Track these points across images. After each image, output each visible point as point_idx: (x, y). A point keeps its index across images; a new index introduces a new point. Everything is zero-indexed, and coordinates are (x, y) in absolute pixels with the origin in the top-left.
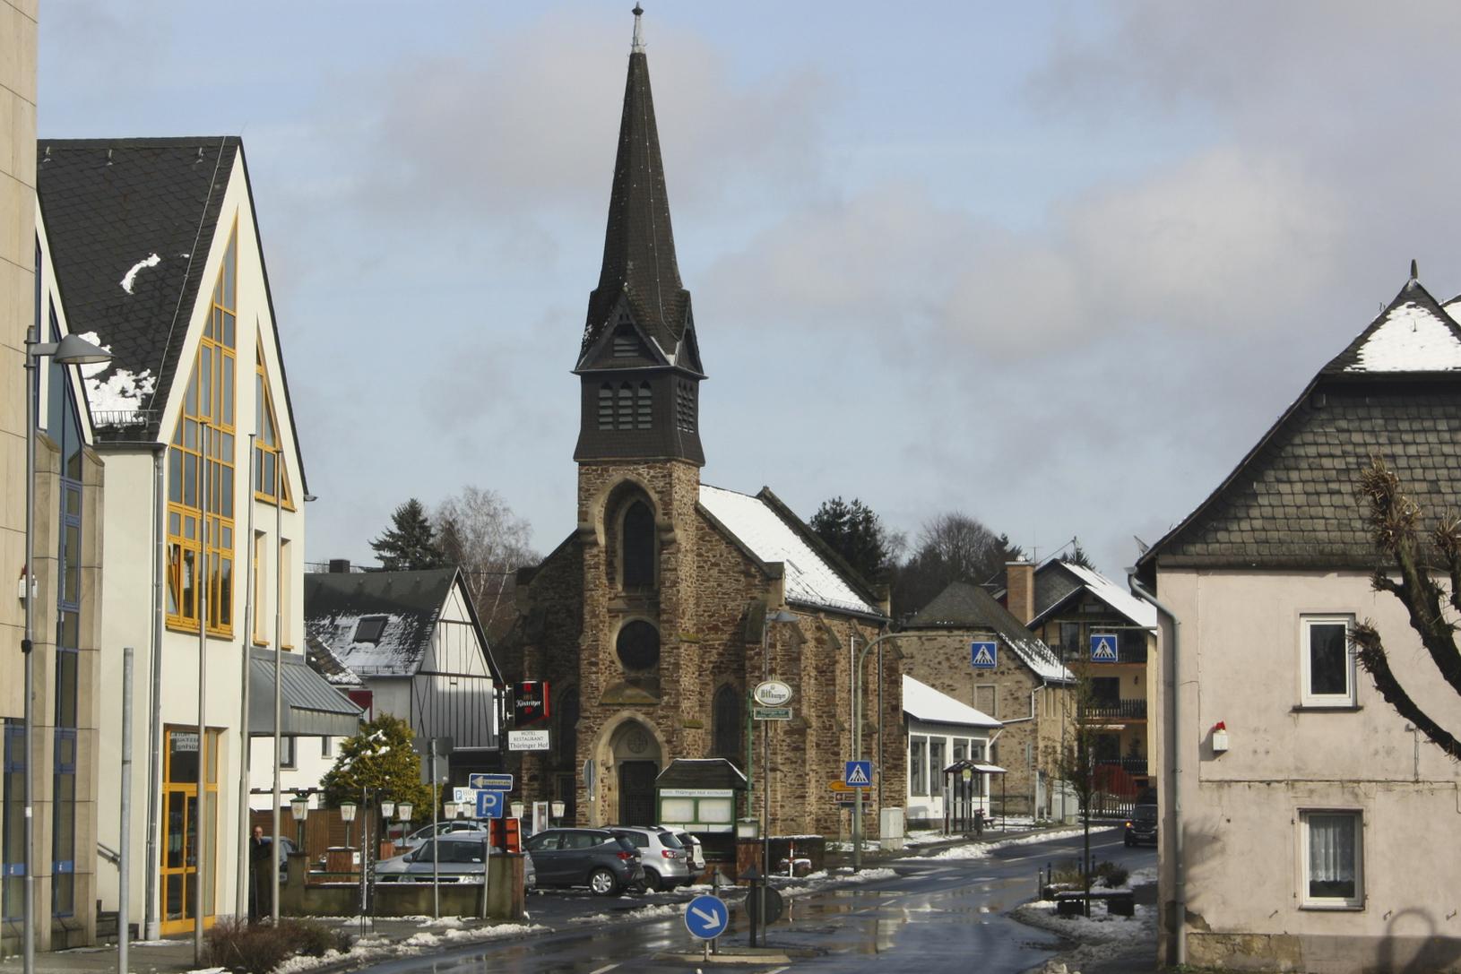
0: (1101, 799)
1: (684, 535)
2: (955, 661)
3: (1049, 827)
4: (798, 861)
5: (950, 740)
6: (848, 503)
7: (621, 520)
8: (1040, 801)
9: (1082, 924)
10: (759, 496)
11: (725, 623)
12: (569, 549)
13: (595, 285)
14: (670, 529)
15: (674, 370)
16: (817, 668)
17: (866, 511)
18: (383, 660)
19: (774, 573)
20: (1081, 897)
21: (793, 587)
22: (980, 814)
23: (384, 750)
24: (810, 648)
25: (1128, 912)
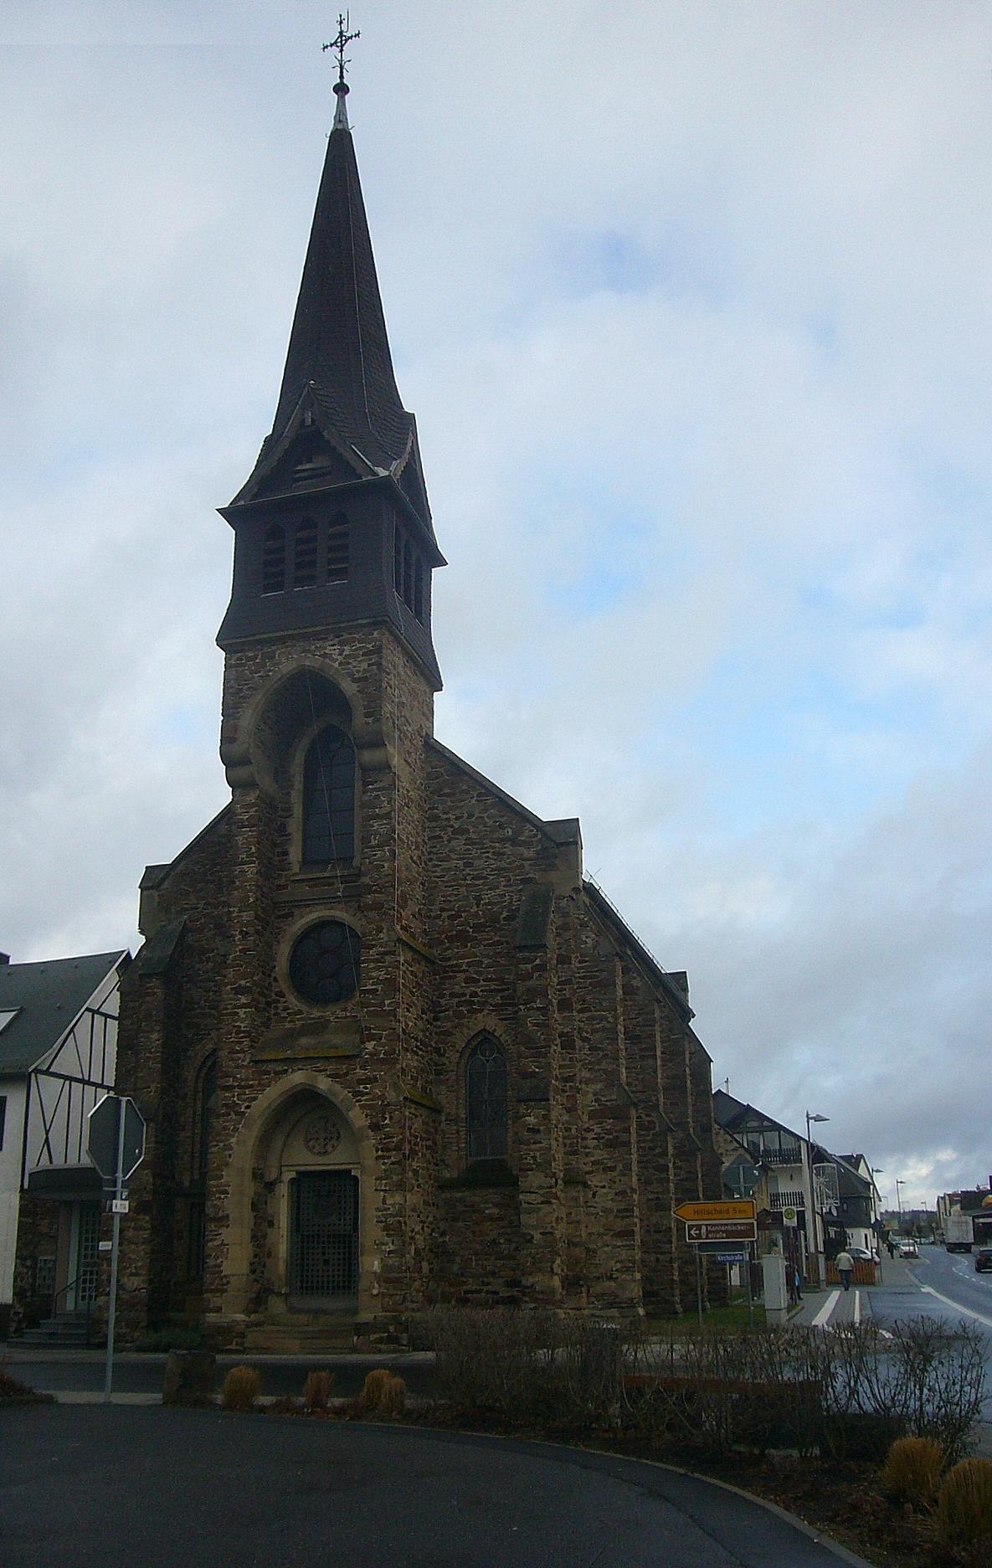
7: (299, 759)
11: (478, 928)
14: (379, 743)
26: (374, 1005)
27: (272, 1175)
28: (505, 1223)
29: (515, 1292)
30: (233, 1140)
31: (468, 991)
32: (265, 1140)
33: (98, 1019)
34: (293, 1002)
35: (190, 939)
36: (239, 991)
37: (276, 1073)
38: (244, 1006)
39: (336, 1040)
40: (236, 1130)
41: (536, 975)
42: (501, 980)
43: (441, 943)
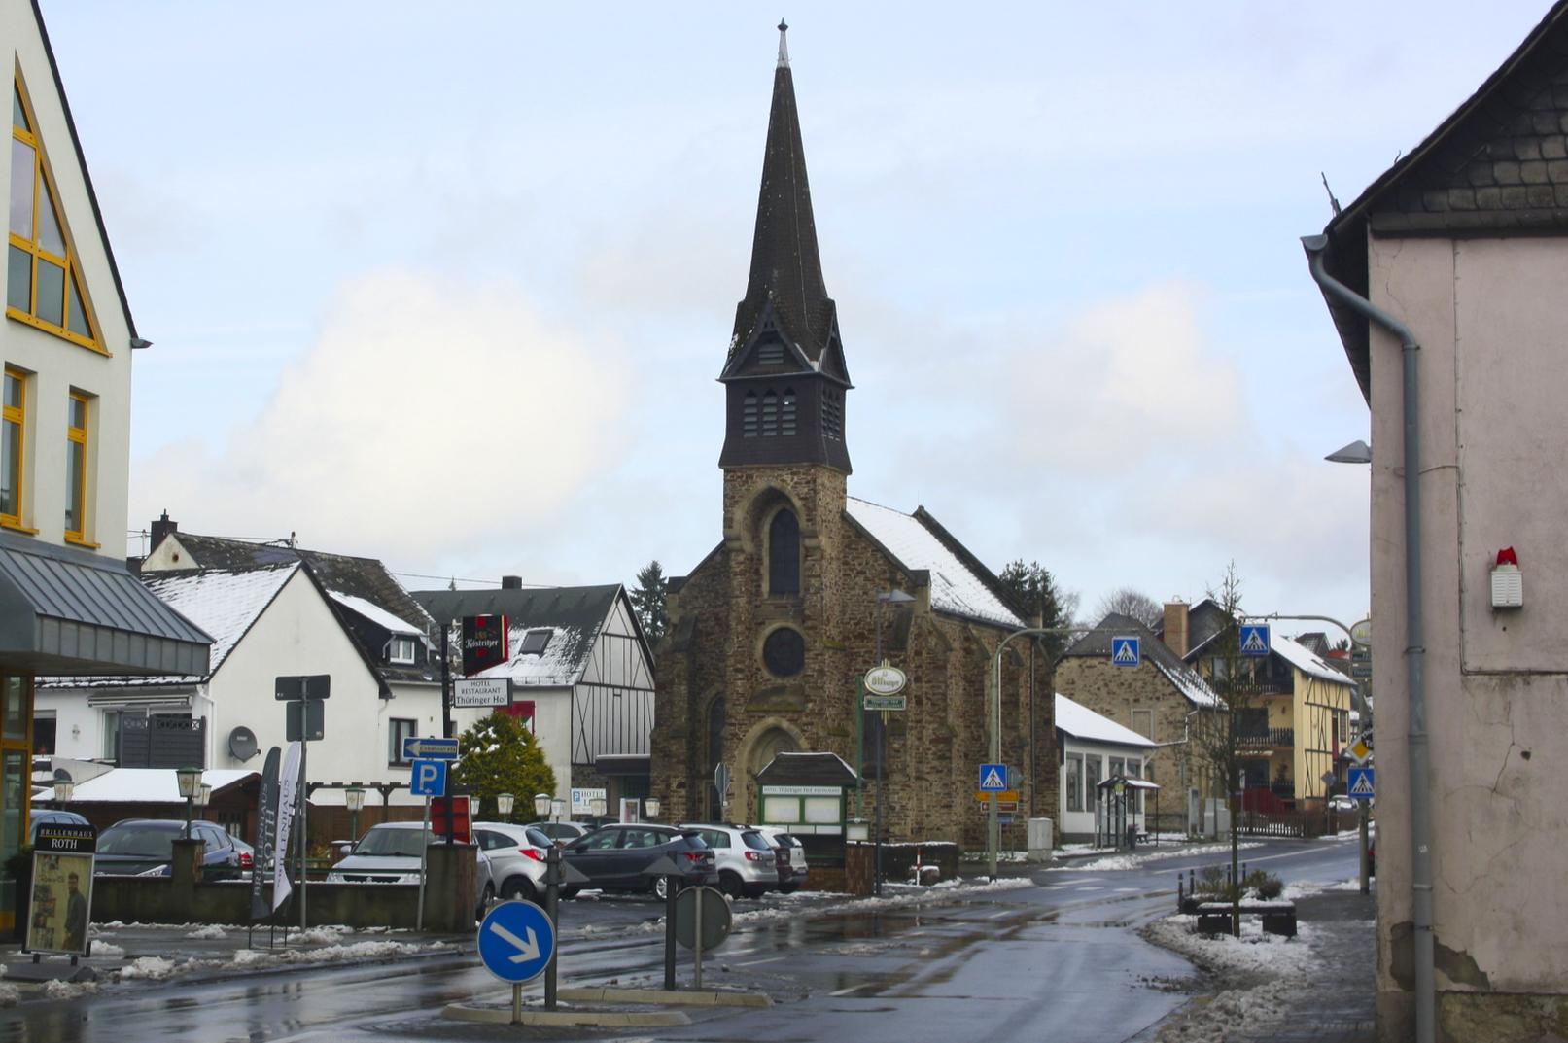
0: (1251, 817)
1: (827, 543)
2: (1113, 687)
3: (1201, 842)
4: (925, 868)
5: (1106, 758)
6: (1028, 566)
7: (766, 528)
8: (1193, 818)
9: (1227, 949)
10: (915, 516)
12: (718, 558)
13: (742, 296)
14: (814, 535)
15: (818, 376)
16: (965, 678)
17: (1044, 572)
18: (546, 671)
19: (919, 581)
20: (1228, 910)
21: (938, 595)
22: (1133, 829)
23: (493, 747)
24: (956, 657)
25: (1289, 931)
32: (753, 752)
34: (766, 673)
36: (738, 670)
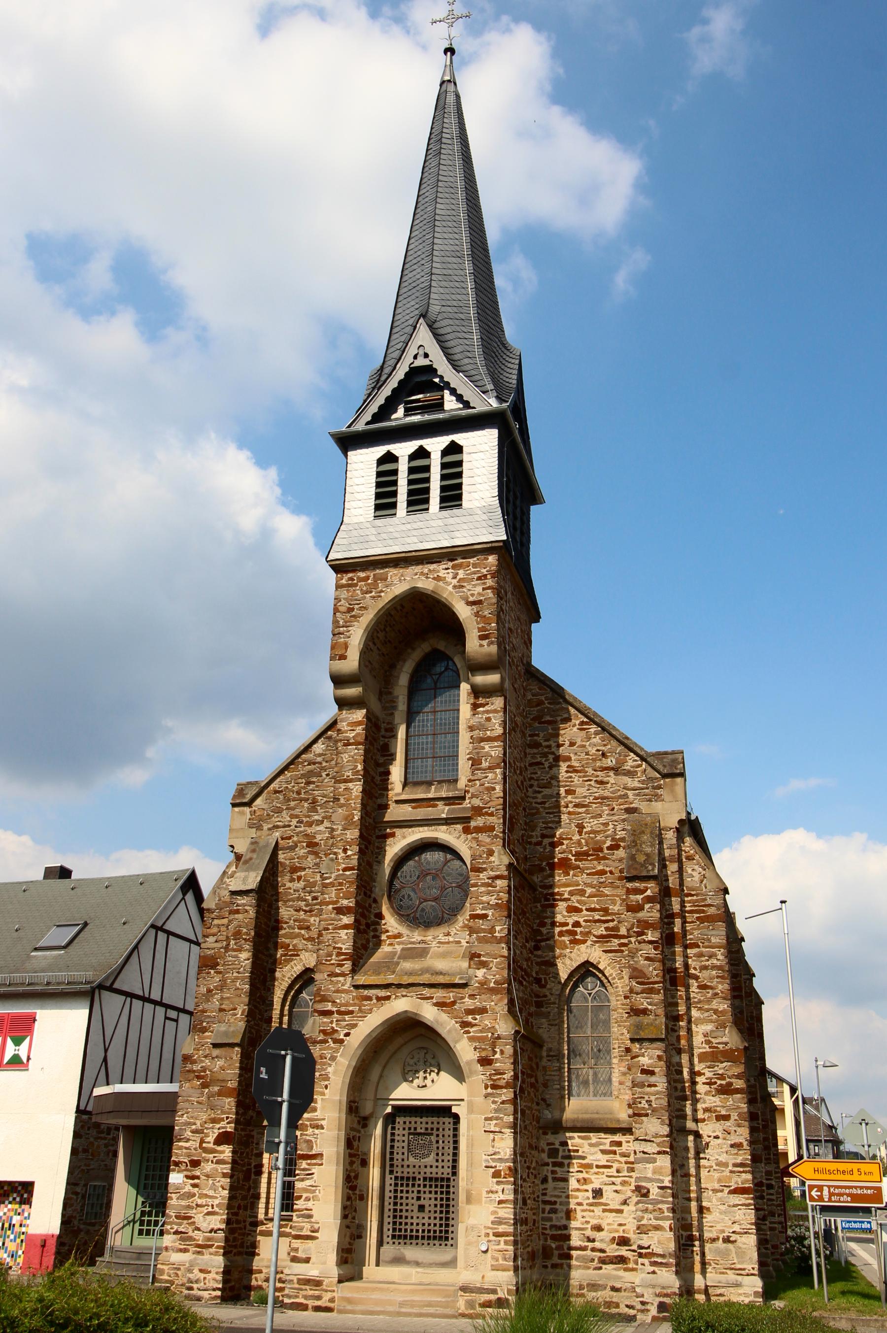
7: (404, 680)
26: (484, 931)
27: (367, 1108)
28: (612, 1171)
29: (623, 1251)
30: (330, 1069)
31: (571, 921)
33: (162, 936)
35: (281, 856)
37: (379, 999)
38: (346, 927)
39: (441, 965)
40: (333, 1058)
41: (647, 906)
42: (606, 911)
43: (542, 870)
